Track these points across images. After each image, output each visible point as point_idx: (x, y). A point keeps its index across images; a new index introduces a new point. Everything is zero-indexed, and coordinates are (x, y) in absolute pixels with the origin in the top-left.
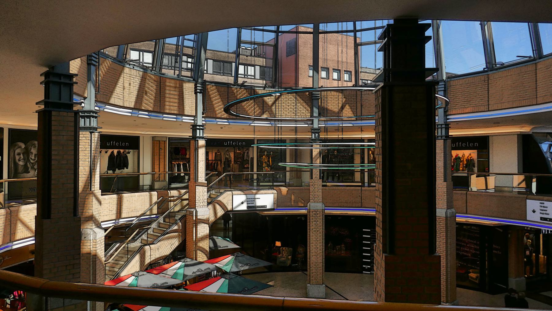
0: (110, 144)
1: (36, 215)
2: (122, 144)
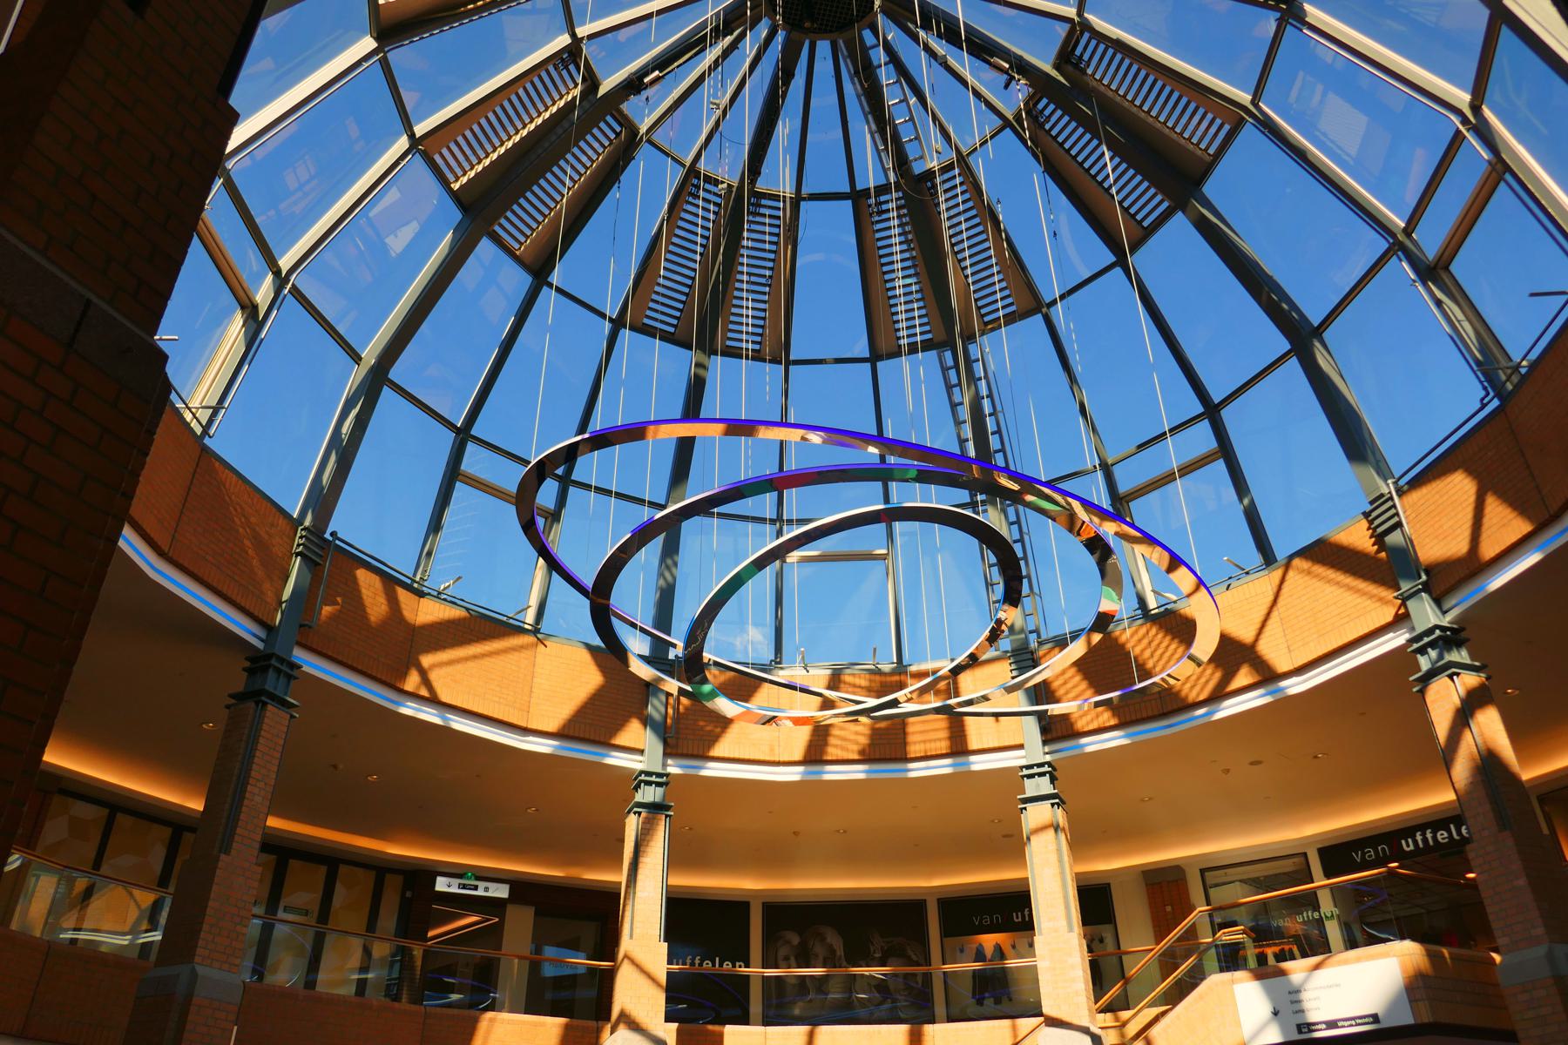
0: (1415, 842)
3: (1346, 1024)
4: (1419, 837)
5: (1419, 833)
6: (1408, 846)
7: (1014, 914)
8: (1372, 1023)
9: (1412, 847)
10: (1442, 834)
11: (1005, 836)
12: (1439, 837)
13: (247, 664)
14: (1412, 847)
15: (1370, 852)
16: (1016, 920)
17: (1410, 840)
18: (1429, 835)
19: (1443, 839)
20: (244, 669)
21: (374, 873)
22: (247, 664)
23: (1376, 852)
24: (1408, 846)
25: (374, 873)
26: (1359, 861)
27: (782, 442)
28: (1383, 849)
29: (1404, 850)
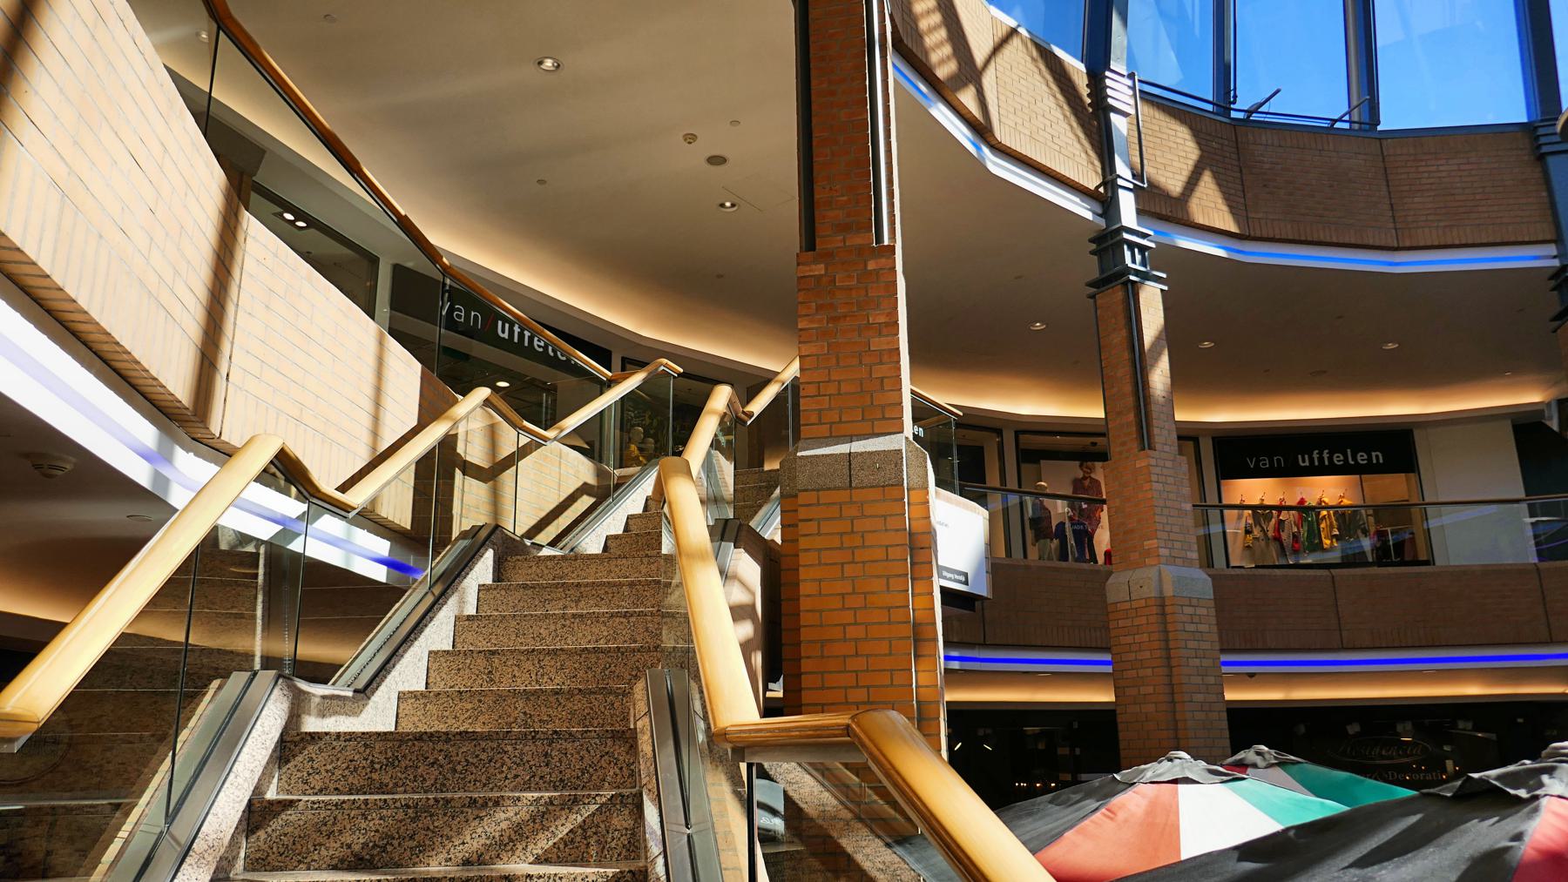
0: (1311, 460)
1: (1476, 820)
2: (1354, 458)
3: (949, 575)
4: (1315, 455)
5: (1317, 451)
6: (1377, 457)
7: (1381, 461)
8: (960, 582)
9: (1307, 464)
10: (1338, 457)
11: (1016, 278)
12: (1335, 460)
13: (1094, 246)
14: (1307, 464)
15: (1362, 460)
16: (1302, 464)
17: (1306, 456)
18: (1326, 455)
19: (1265, 460)
20: (1092, 253)
21: (1222, 481)
22: (1094, 246)
23: (1271, 462)
24: (1377, 457)
25: (1222, 481)
26: (1252, 467)
27: (1180, 438)
28: (1278, 460)
29: (1299, 465)
